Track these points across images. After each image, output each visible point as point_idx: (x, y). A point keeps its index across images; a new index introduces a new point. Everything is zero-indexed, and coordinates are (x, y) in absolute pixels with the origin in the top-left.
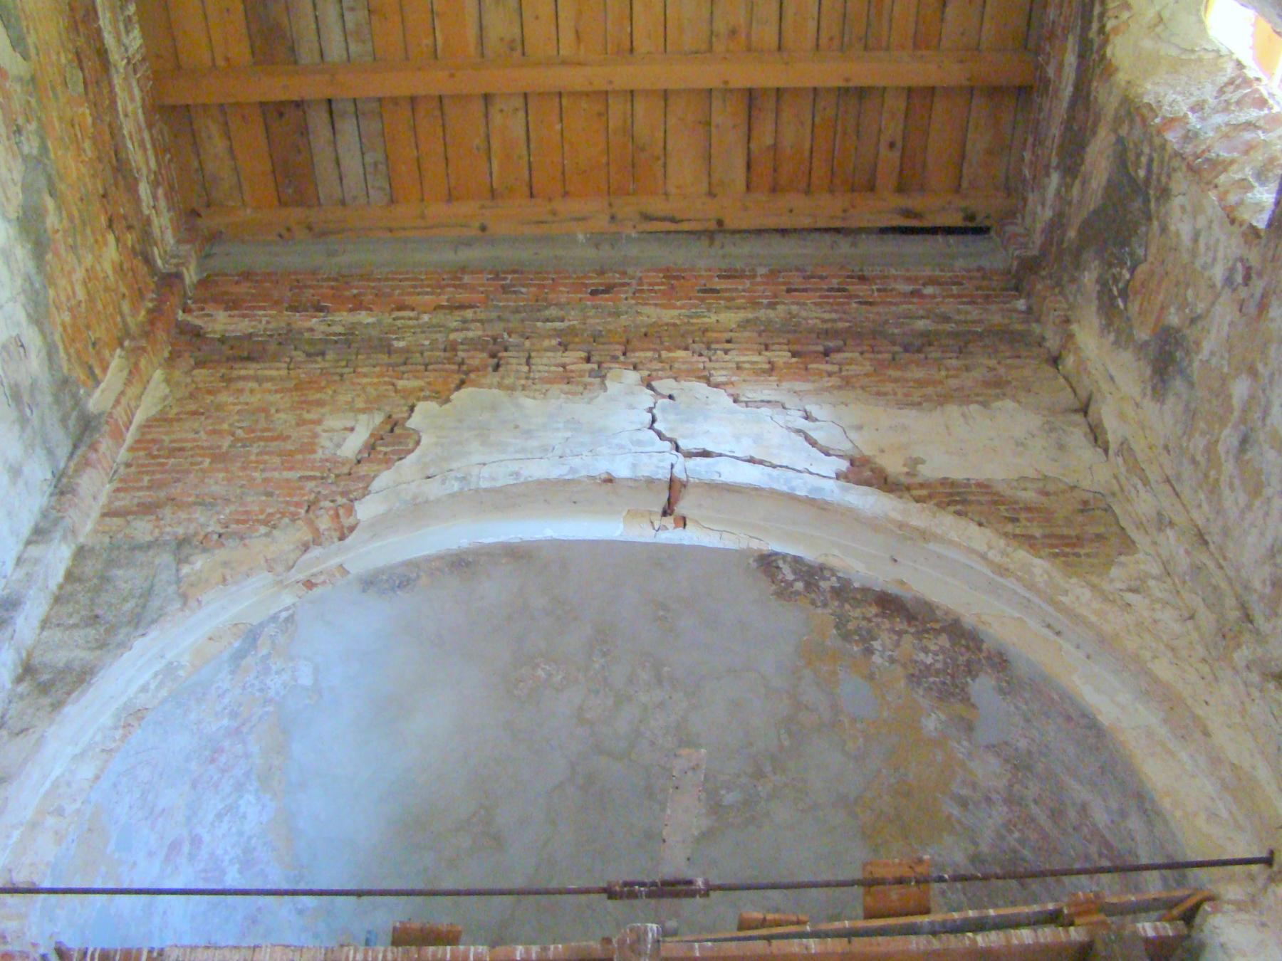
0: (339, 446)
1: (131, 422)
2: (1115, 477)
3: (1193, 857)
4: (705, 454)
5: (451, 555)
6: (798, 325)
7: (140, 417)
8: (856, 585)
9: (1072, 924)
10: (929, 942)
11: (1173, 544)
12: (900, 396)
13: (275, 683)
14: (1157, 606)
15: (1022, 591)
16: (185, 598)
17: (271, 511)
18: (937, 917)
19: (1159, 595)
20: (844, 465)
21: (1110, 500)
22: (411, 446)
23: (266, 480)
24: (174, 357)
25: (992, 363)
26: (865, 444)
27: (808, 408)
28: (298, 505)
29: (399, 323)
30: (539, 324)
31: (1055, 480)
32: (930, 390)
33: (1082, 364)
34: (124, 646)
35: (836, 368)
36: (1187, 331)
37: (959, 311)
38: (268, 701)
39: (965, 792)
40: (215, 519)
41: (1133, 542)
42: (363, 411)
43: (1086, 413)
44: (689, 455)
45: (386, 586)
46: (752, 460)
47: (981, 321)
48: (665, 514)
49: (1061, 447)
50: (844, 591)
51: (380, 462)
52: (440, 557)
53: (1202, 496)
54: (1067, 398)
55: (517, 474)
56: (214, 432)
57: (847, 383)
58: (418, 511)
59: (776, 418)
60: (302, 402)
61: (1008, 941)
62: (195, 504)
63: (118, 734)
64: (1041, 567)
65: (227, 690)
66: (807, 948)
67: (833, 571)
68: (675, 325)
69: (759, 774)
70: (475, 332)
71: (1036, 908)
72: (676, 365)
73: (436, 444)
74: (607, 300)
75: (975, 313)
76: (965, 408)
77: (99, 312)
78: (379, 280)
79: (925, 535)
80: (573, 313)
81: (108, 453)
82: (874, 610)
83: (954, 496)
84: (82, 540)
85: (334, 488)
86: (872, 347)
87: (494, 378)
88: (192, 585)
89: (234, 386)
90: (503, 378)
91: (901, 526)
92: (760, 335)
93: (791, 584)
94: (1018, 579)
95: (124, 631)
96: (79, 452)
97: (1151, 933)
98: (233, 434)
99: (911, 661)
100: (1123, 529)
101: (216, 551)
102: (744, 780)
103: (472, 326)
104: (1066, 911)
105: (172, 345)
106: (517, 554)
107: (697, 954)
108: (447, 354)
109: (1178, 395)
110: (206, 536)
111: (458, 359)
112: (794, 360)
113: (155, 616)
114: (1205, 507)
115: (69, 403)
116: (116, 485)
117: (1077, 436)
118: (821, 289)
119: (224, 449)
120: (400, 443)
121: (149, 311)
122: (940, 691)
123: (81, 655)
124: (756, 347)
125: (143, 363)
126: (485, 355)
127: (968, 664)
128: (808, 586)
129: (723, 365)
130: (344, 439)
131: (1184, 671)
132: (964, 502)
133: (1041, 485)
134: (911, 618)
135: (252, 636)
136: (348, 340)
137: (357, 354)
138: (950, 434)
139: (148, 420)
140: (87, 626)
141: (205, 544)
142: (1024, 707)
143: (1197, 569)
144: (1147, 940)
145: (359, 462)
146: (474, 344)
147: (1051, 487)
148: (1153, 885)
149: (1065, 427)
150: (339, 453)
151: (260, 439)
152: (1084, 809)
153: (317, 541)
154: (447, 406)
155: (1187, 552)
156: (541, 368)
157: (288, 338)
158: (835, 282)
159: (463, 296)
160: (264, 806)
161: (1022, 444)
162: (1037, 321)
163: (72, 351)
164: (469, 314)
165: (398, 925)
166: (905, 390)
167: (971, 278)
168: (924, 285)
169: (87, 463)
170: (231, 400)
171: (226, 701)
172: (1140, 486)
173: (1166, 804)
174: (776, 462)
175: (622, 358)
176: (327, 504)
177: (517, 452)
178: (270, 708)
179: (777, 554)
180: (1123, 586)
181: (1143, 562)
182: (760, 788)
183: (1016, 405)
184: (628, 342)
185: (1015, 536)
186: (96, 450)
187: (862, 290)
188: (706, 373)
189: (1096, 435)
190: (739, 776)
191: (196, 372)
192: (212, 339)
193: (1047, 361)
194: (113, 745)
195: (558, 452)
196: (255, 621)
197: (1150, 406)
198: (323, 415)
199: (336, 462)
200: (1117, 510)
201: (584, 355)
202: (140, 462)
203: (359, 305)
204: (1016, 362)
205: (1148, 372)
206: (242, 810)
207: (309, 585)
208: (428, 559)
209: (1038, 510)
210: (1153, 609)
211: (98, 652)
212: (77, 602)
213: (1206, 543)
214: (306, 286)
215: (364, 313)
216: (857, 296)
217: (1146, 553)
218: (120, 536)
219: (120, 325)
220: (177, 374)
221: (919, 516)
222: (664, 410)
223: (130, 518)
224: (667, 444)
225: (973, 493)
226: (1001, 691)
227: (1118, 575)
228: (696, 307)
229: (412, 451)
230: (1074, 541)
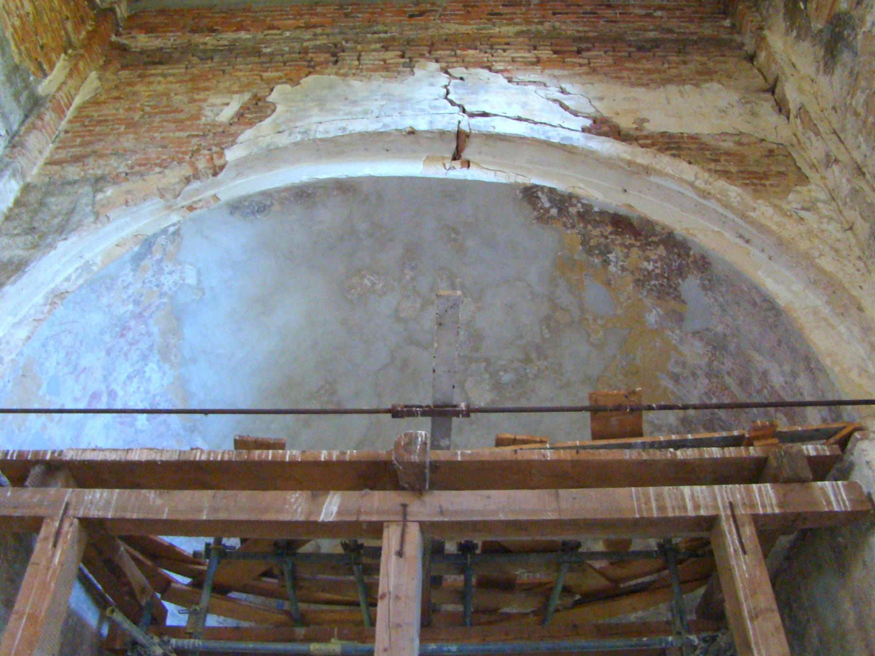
0: (217, 115)
1: (71, 105)
2: (795, 135)
3: (844, 398)
4: (485, 115)
5: (295, 187)
6: (559, 34)
7: (77, 101)
8: (596, 209)
9: (752, 445)
10: (639, 454)
11: (837, 176)
12: (633, 79)
13: (168, 281)
14: (825, 220)
15: (721, 210)
16: (97, 215)
17: (164, 157)
18: (647, 439)
19: (825, 212)
20: (588, 123)
21: (790, 150)
22: (269, 112)
23: (163, 138)
24: (107, 63)
25: (704, 59)
26: (604, 109)
27: (563, 86)
28: (185, 153)
29: (268, 37)
30: (369, 36)
31: (749, 135)
32: (655, 76)
33: (771, 56)
34: (52, 246)
35: (586, 61)
36: (854, 13)
37: (680, 27)
38: (163, 295)
39: (677, 370)
40: (124, 163)
41: (807, 178)
42: (236, 92)
43: (773, 93)
44: (472, 115)
45: (248, 211)
46: (519, 119)
47: (695, 33)
48: (454, 159)
49: (754, 114)
50: (587, 215)
51: (246, 124)
52: (287, 189)
53: (861, 139)
54: (760, 82)
55: (344, 129)
56: (129, 109)
57: (594, 71)
58: (271, 156)
59: (539, 92)
60: (194, 89)
61: (701, 455)
62: (111, 154)
63: (46, 309)
64: (734, 192)
65: (130, 283)
66: (544, 456)
67: (578, 198)
68: (468, 34)
69: (527, 360)
70: (322, 41)
71: (724, 434)
72: (467, 59)
73: (287, 111)
74: (421, 20)
75: (692, 28)
76: (682, 88)
77: (45, 25)
78: (257, 12)
79: (648, 170)
80: (394, 28)
81: (52, 123)
82: (609, 229)
83: (670, 144)
84: (29, 180)
85: (211, 142)
86: (614, 48)
87: (332, 69)
88: (103, 206)
89: (146, 80)
90: (339, 69)
91: (630, 163)
92: (530, 40)
93: (547, 211)
94: (719, 200)
95: (51, 237)
96: (30, 120)
97: (812, 453)
98: (143, 110)
99: (637, 268)
100: (799, 169)
101: (123, 184)
102: (517, 364)
103: (321, 38)
104: (747, 436)
105: (106, 56)
106: (345, 188)
107: (459, 459)
108: (301, 56)
109: (844, 65)
110: (117, 175)
111: (308, 58)
112: (555, 56)
113: (74, 227)
114: (864, 147)
115: (20, 85)
116: (57, 144)
117: (766, 107)
118: (576, 13)
119: (136, 119)
120: (262, 112)
121: (88, 32)
122: (659, 293)
123: (19, 253)
124: (527, 47)
125: (81, 65)
126: (328, 55)
127: (680, 268)
128: (560, 211)
129: (501, 59)
130: (221, 111)
131: (845, 265)
132: (679, 148)
133: (737, 138)
134: (637, 234)
135: (148, 244)
136: (231, 49)
137: (236, 58)
138: (669, 103)
139: (84, 103)
140: (27, 234)
141: (116, 179)
142: (721, 299)
143: (855, 192)
144: (810, 459)
145: (231, 124)
146: (319, 49)
147: (745, 140)
148: (814, 418)
149: (757, 101)
150: (217, 119)
151: (162, 112)
152: (765, 375)
153: (196, 176)
154: (298, 87)
155: (848, 180)
156: (367, 62)
157: (188, 50)
158: (588, 8)
159: (315, 20)
160: (164, 374)
161: (724, 111)
162: (739, 33)
163: (23, 48)
164: (319, 30)
165: (237, 438)
166: (637, 76)
167: (690, 6)
168: (655, 10)
169: (34, 127)
170: (144, 88)
171: (130, 291)
172: (813, 138)
173: (828, 362)
174: (537, 120)
175: (427, 55)
176: (206, 152)
177: (346, 115)
178: (165, 300)
179: (536, 186)
180: (799, 206)
181: (815, 190)
182: (528, 371)
183: (720, 86)
184: (433, 44)
185: (716, 171)
186: (42, 119)
187: (609, 13)
188: (489, 64)
189: (781, 107)
190: (513, 362)
191: (121, 73)
192: (135, 52)
193: (745, 58)
194: (42, 316)
195: (377, 114)
196: (150, 232)
197: (823, 80)
198: (209, 95)
199: (214, 125)
200: (794, 155)
201: (399, 53)
202: (75, 130)
203: (240, 27)
204: (721, 59)
205: (822, 53)
206: (147, 374)
207: (191, 208)
208: (279, 191)
209: (735, 154)
210: (821, 223)
211: (32, 251)
212: (21, 219)
213: (864, 174)
214: (204, 17)
215: (243, 32)
216: (603, 17)
217: (818, 185)
218: (56, 177)
219: (64, 39)
220: (108, 75)
221: (643, 157)
222: (455, 86)
223: (64, 165)
224: (457, 108)
225: (685, 143)
226: (704, 287)
227: (794, 200)
228: (485, 24)
229: (270, 116)
230: (762, 175)
